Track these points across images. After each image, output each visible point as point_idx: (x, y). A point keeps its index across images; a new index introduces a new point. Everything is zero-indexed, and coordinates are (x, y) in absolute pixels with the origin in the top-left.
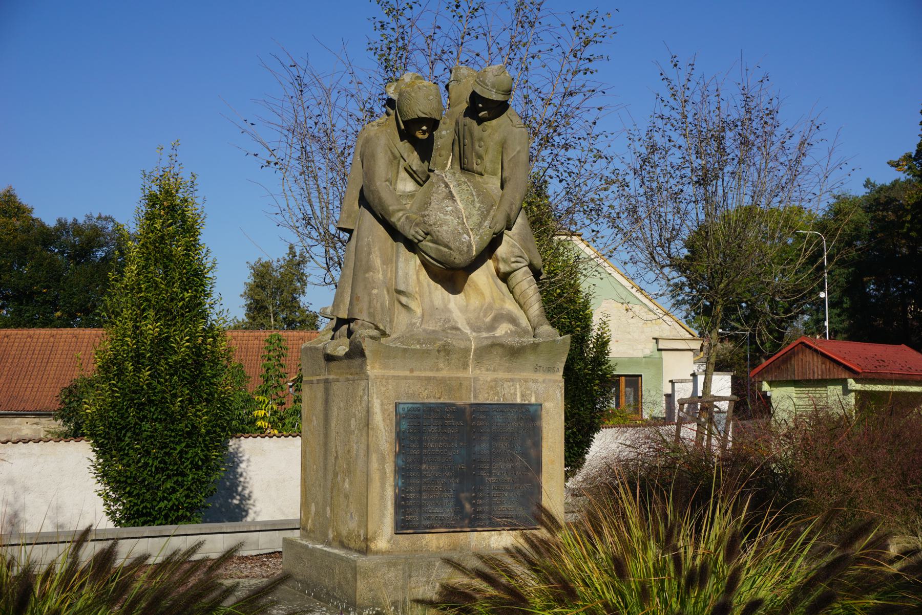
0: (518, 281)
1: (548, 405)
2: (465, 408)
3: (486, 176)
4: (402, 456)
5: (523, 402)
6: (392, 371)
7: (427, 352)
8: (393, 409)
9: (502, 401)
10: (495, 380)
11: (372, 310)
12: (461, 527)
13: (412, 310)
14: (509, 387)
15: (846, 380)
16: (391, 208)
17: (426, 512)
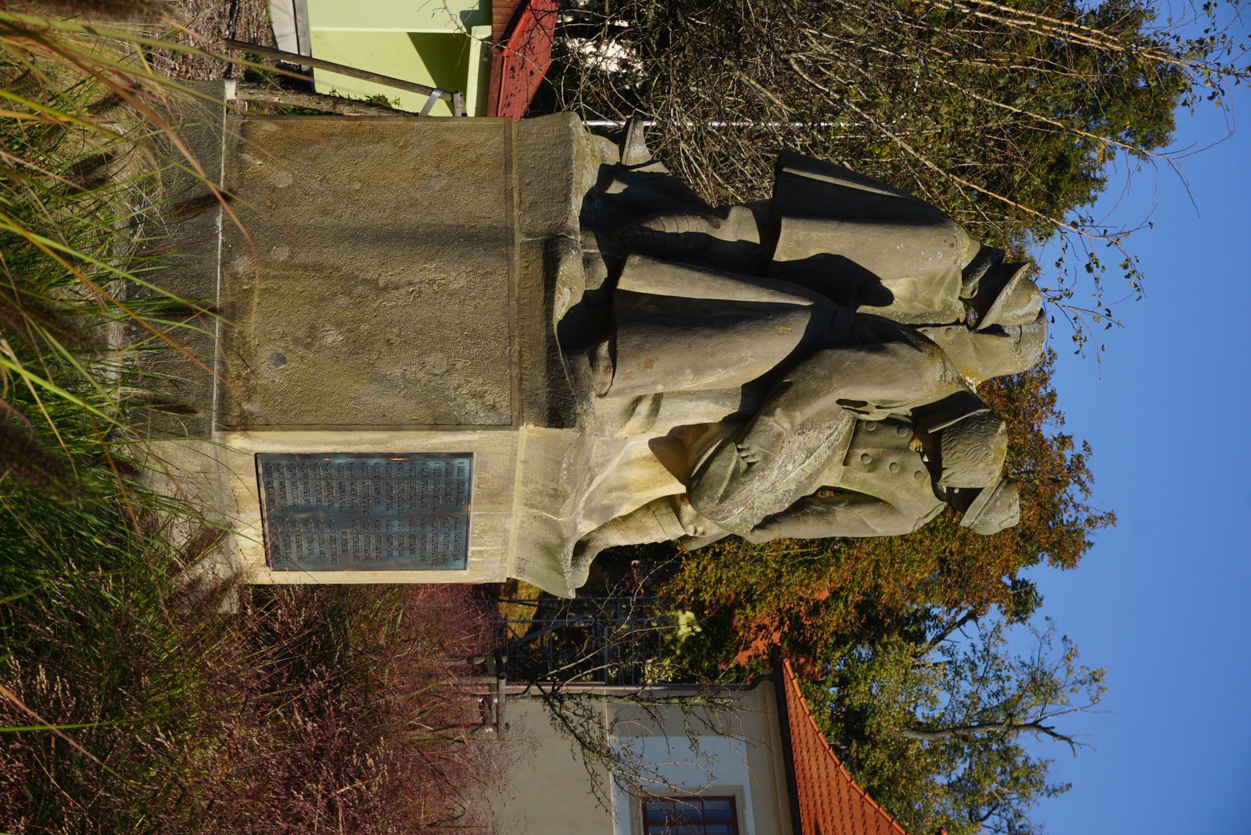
0: (665, 528)
3: (843, 467)
13: (625, 423)
15: (488, 21)
16: (798, 414)
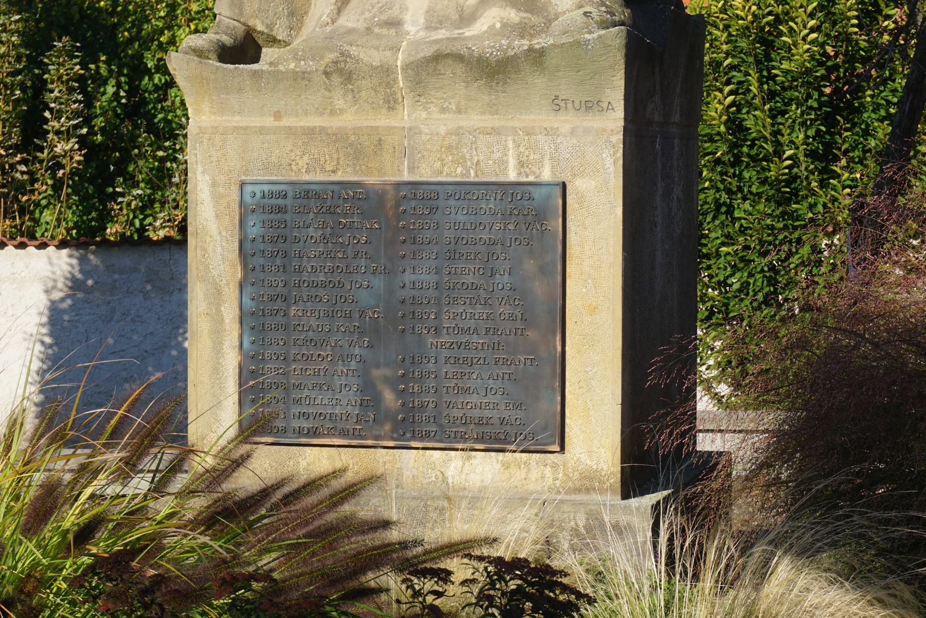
1: (578, 187)
5: (524, 179)
6: (237, 118)
8: (235, 195)
9: (472, 178)
10: (458, 132)
12: (377, 438)
17: (298, 401)
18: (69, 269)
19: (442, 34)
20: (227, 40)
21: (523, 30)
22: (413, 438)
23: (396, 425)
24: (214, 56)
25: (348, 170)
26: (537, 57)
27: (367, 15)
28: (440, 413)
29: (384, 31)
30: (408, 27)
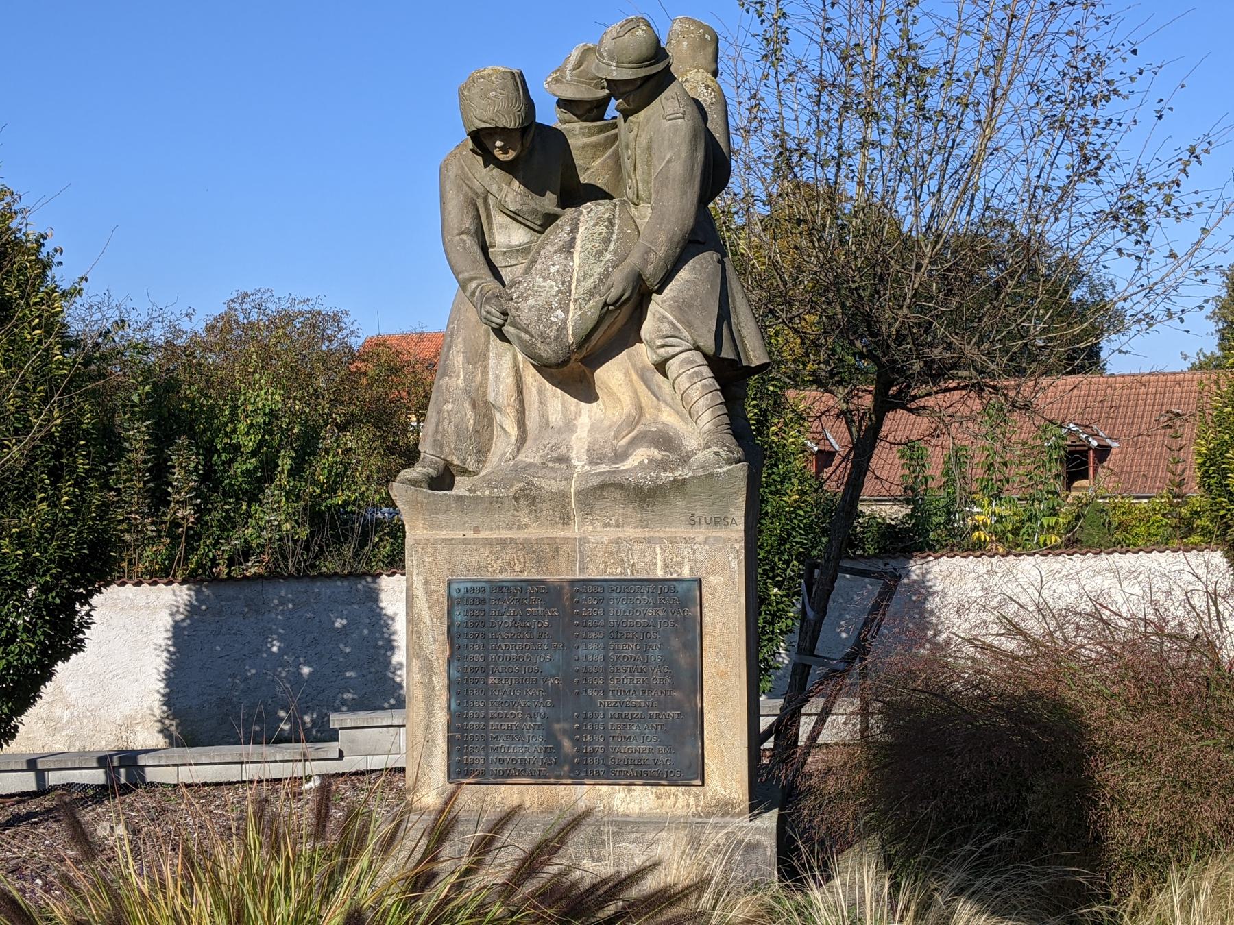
1: (712, 581)
2: (562, 588)
4: (456, 663)
5: (669, 577)
6: (444, 532)
7: (498, 500)
8: (443, 591)
10: (617, 541)
11: (439, 437)
12: (558, 777)
14: (642, 552)
17: (495, 750)
18: (188, 598)
19: (603, 468)
20: (433, 472)
21: (665, 465)
22: (587, 777)
23: (573, 767)
24: (426, 485)
25: (533, 570)
26: (679, 486)
27: (541, 453)
28: (608, 757)
29: (557, 465)
30: (575, 462)
